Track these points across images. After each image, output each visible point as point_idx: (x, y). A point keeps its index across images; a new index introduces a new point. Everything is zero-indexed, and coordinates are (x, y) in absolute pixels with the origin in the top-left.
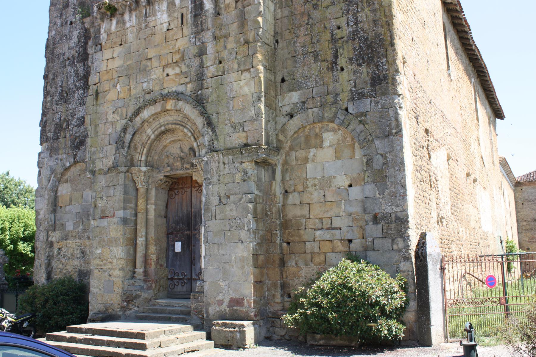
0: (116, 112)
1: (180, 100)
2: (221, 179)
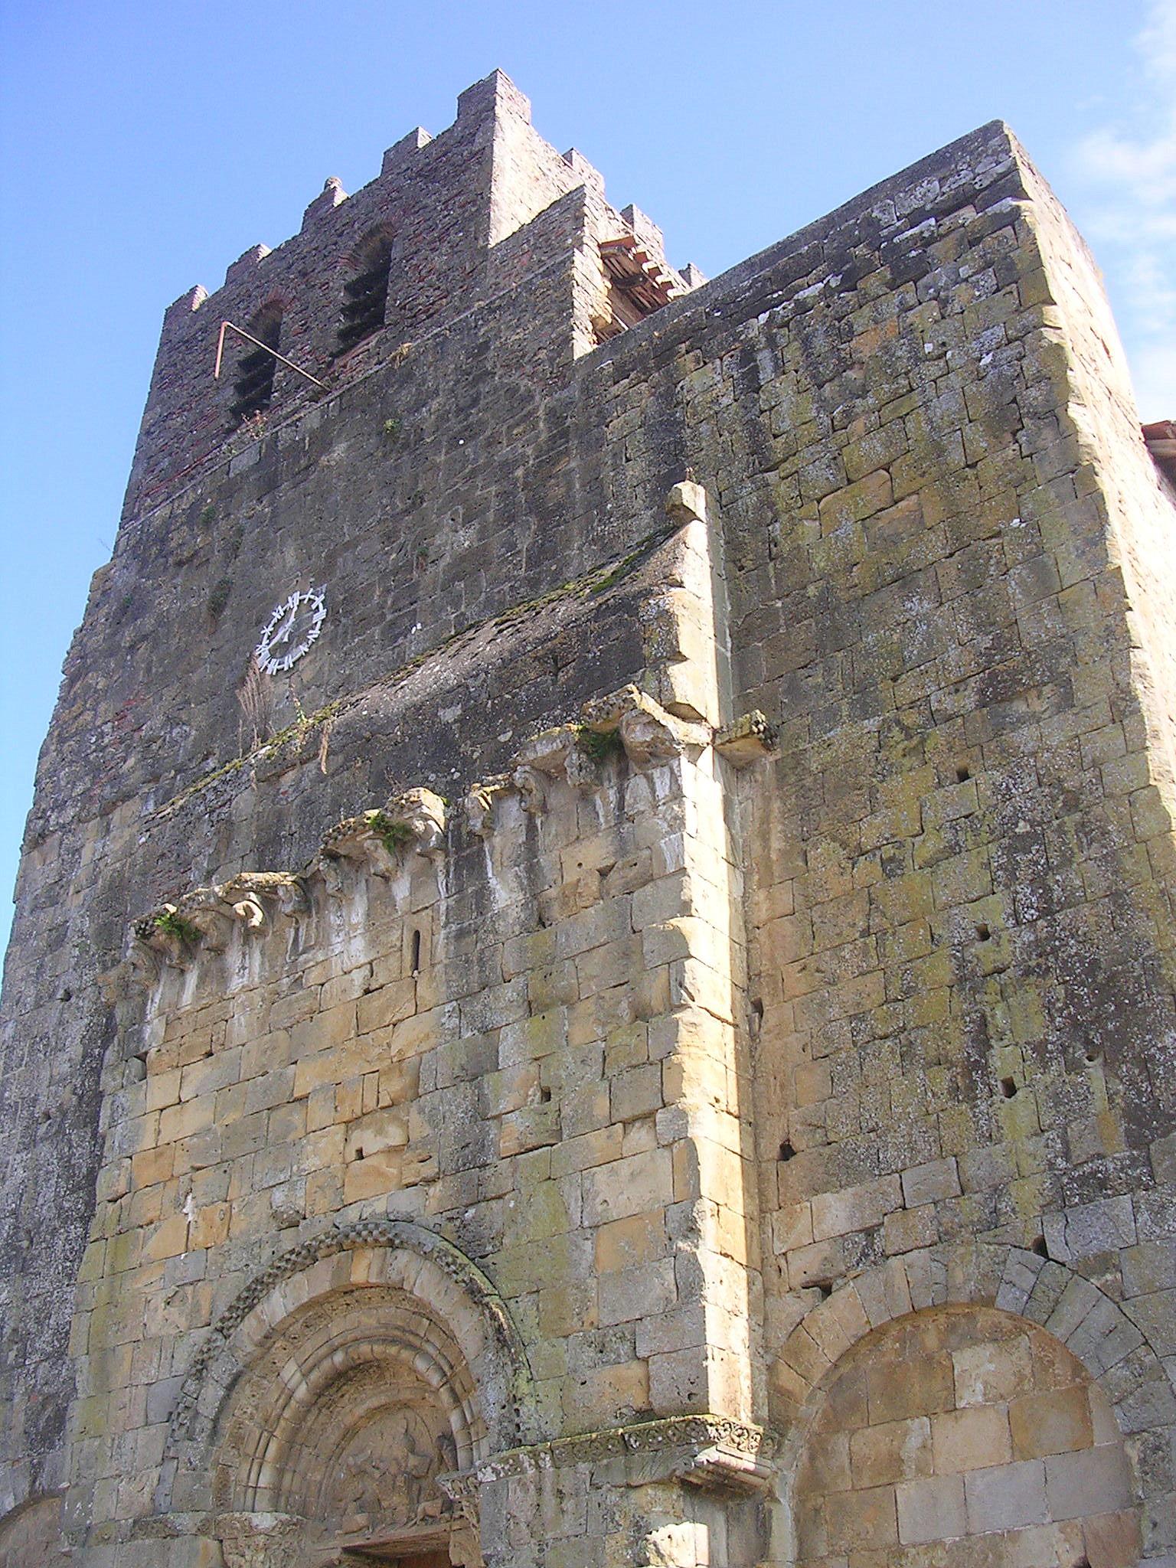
0: (177, 1301)
1: (402, 1246)
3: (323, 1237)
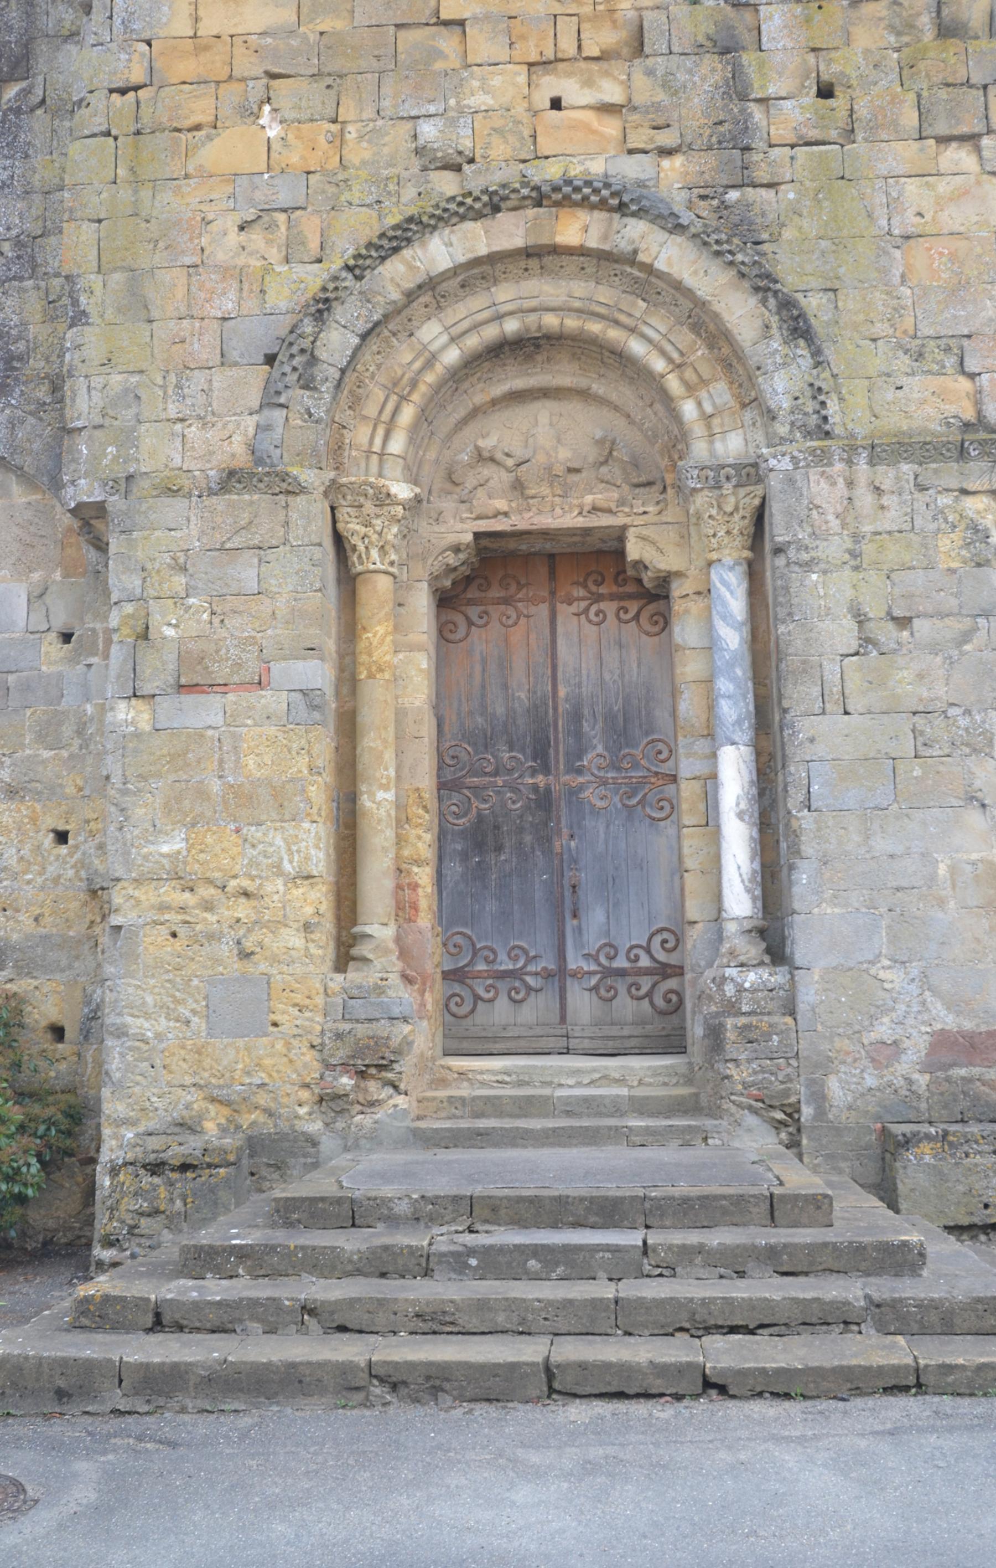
2: (868, 548)
3: (517, 186)
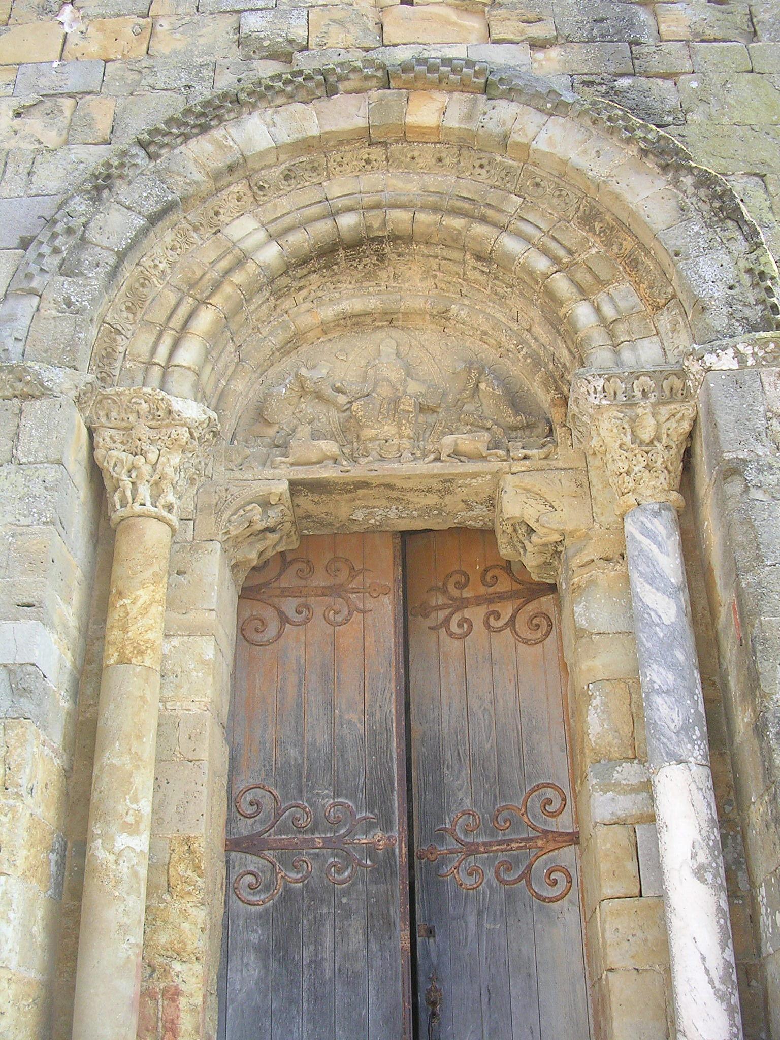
3: (359, 64)
